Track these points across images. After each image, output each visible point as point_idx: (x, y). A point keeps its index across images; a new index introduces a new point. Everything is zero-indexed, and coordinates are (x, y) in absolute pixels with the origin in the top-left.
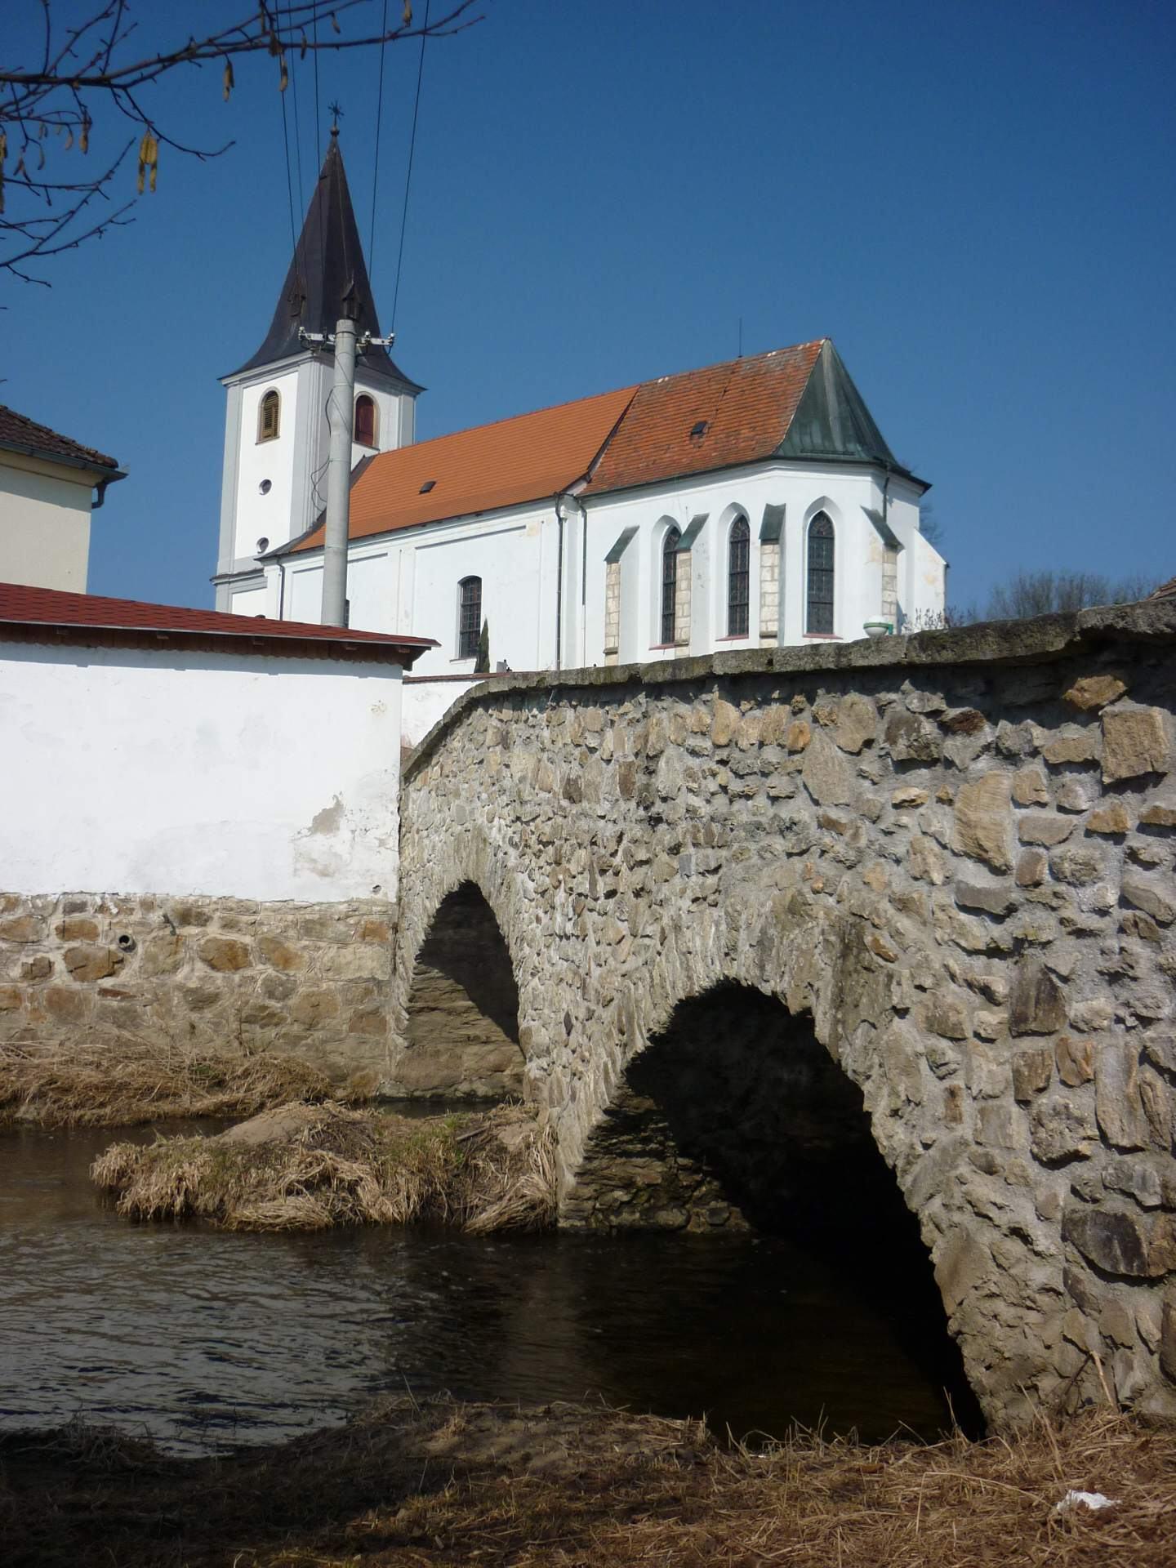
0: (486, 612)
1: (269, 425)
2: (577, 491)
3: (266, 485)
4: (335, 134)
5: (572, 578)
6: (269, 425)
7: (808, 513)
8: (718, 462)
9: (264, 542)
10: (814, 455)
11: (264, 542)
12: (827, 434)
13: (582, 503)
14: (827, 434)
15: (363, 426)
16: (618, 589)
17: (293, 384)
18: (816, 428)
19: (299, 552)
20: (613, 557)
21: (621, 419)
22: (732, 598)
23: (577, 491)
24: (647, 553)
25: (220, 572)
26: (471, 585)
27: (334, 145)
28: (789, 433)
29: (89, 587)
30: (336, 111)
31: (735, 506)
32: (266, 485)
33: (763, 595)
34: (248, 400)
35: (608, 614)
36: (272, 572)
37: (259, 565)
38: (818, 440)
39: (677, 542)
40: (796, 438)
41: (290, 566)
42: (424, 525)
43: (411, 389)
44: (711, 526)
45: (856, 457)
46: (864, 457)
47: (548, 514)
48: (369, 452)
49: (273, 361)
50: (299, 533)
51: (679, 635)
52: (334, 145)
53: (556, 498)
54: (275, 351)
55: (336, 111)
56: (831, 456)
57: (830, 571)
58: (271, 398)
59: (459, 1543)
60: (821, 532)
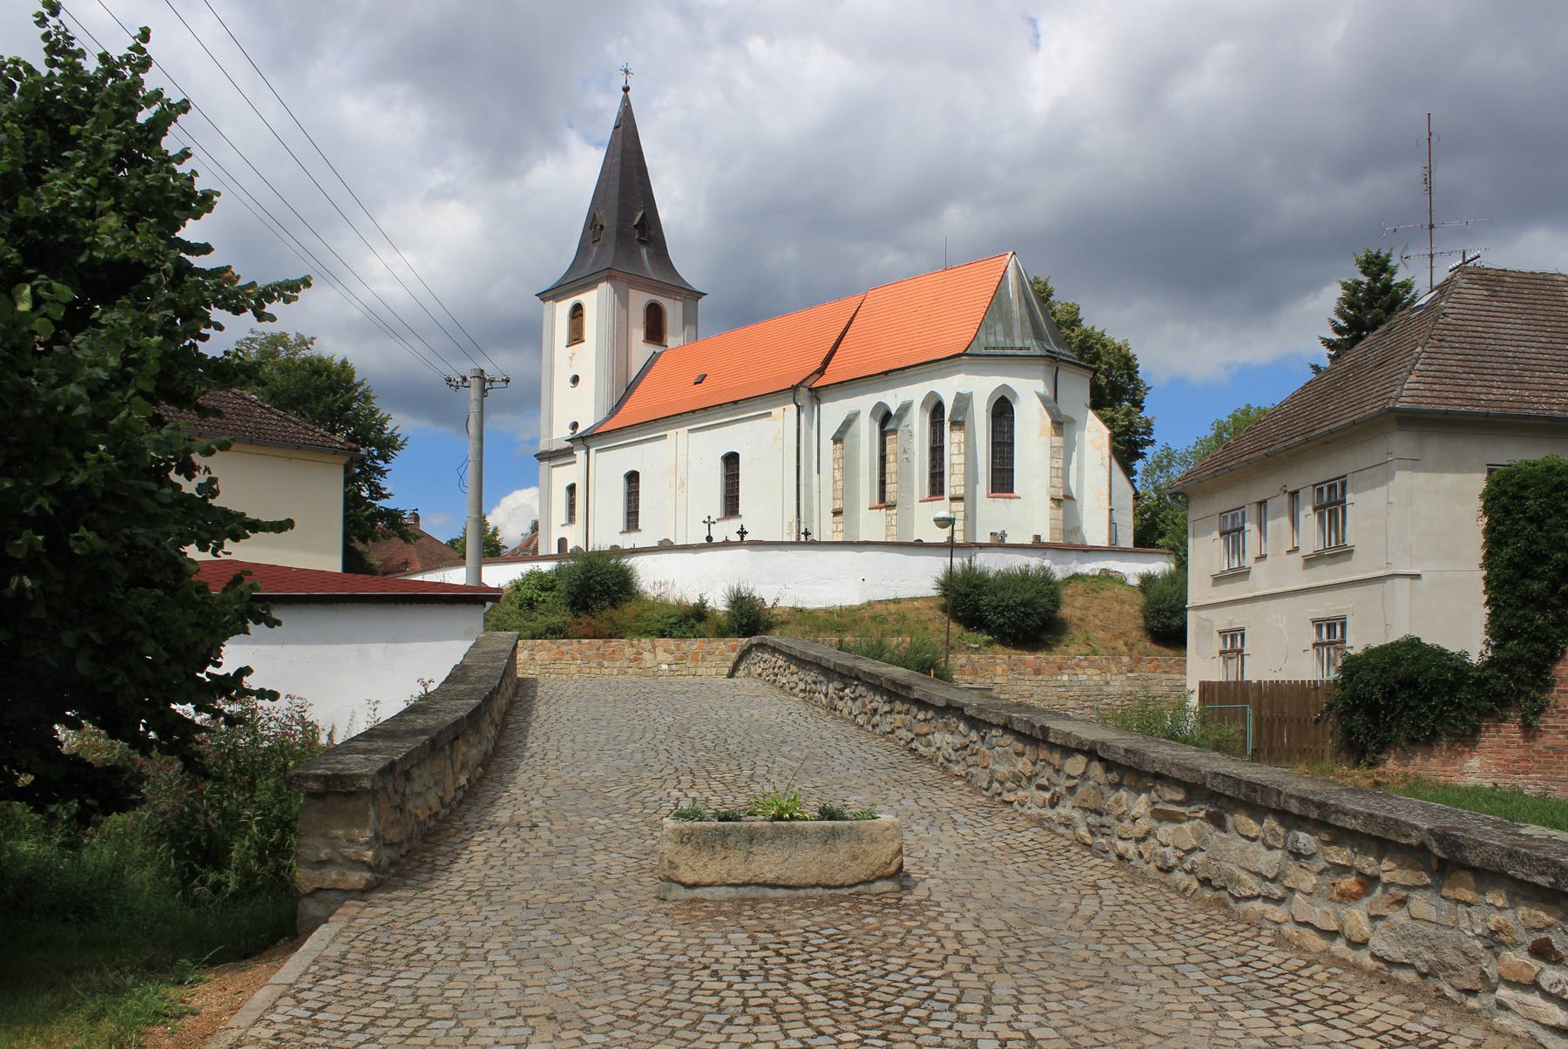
1: (576, 336)
3: (575, 380)
5: (808, 451)
6: (576, 336)
9: (575, 426)
11: (575, 426)
12: (1009, 333)
14: (1009, 333)
16: (847, 466)
20: (837, 439)
22: (637, 500)
24: (866, 430)
27: (626, 99)
29: (598, 145)
31: (933, 394)
32: (575, 380)
33: (952, 465)
35: (835, 482)
38: (1001, 338)
39: (886, 420)
40: (982, 336)
45: (1031, 352)
46: (1039, 352)
50: (601, 418)
51: (889, 498)
52: (626, 99)
56: (1009, 352)
57: (637, 493)
60: (1002, 410)
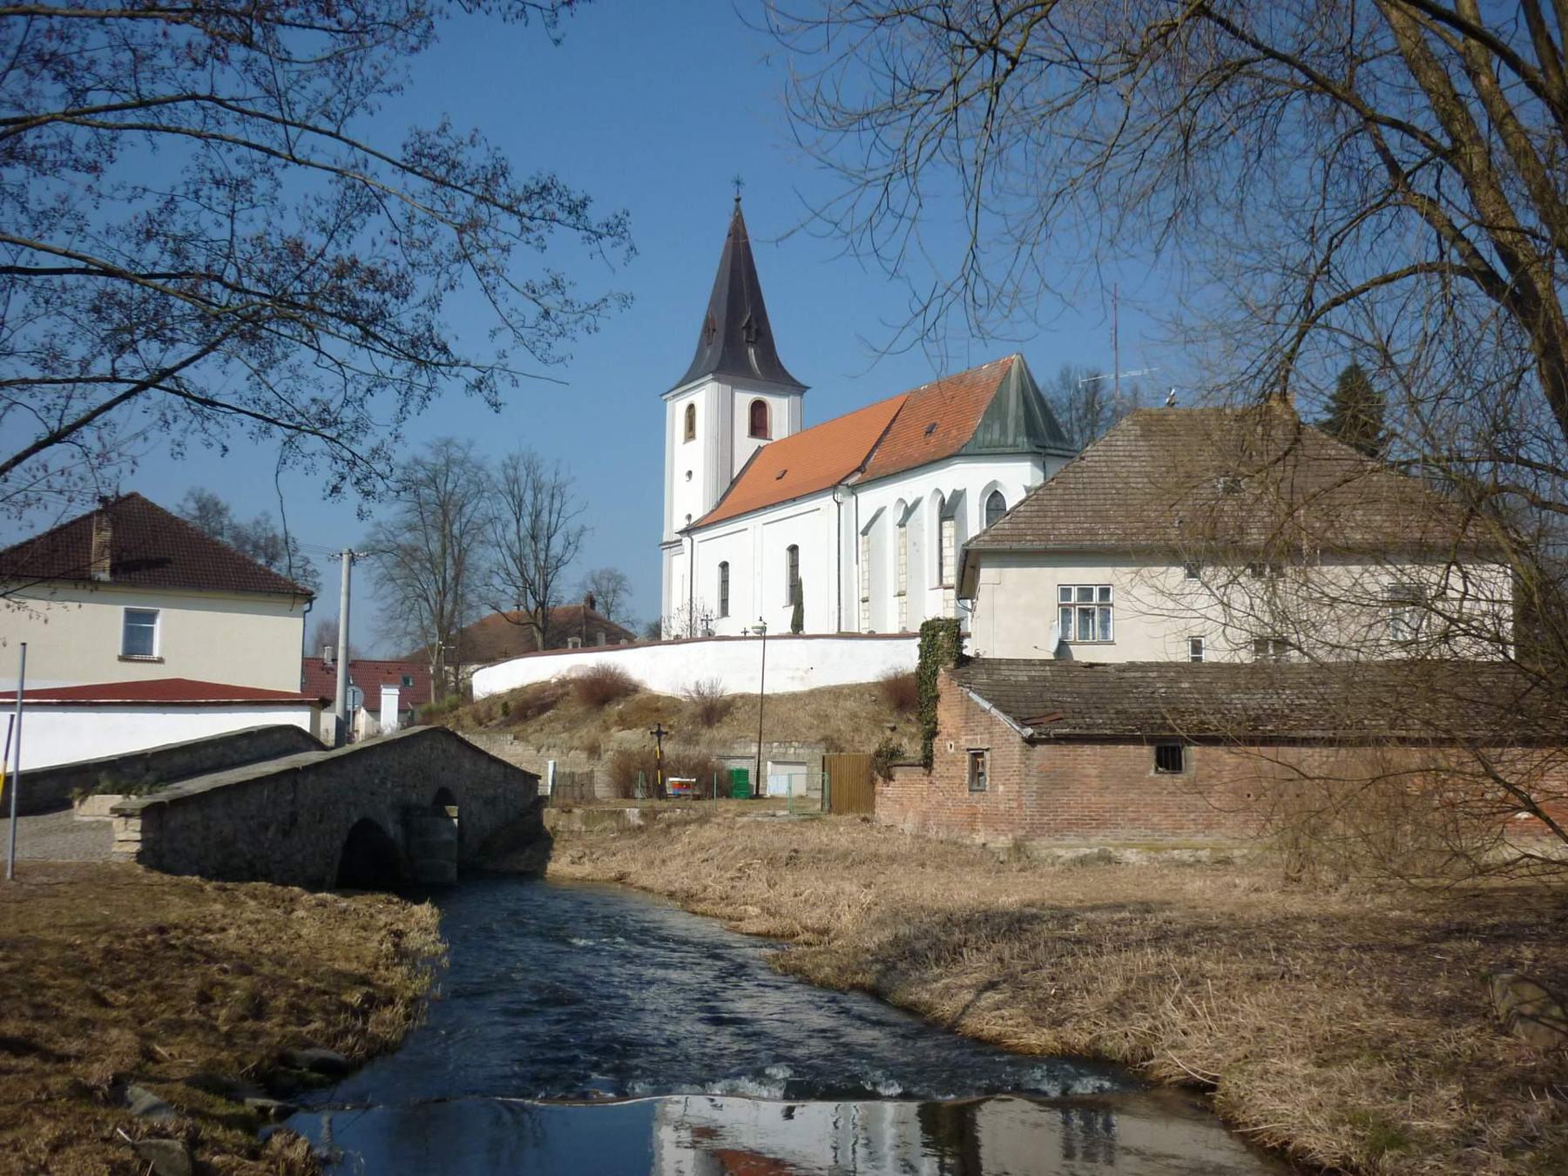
0: (801, 573)
2: (851, 481)
3: (690, 474)
4: (738, 200)
7: (983, 494)
8: (921, 461)
9: (689, 517)
10: (992, 450)
11: (689, 517)
12: (1004, 431)
13: (854, 489)
14: (1004, 431)
15: (759, 422)
17: (704, 396)
18: (997, 427)
19: (715, 523)
21: (894, 420)
23: (851, 481)
25: (665, 539)
26: (793, 549)
27: (738, 209)
28: (975, 433)
30: (738, 183)
32: (690, 474)
34: (678, 409)
36: (686, 541)
37: (678, 537)
38: (996, 436)
41: (697, 537)
42: (765, 508)
43: (797, 388)
44: (924, 505)
47: (826, 502)
48: (762, 443)
49: (259, 781)
52: (738, 209)
53: (834, 488)
54: (691, 377)
55: (738, 183)
56: (999, 450)
58: (691, 407)
59: (151, 11)
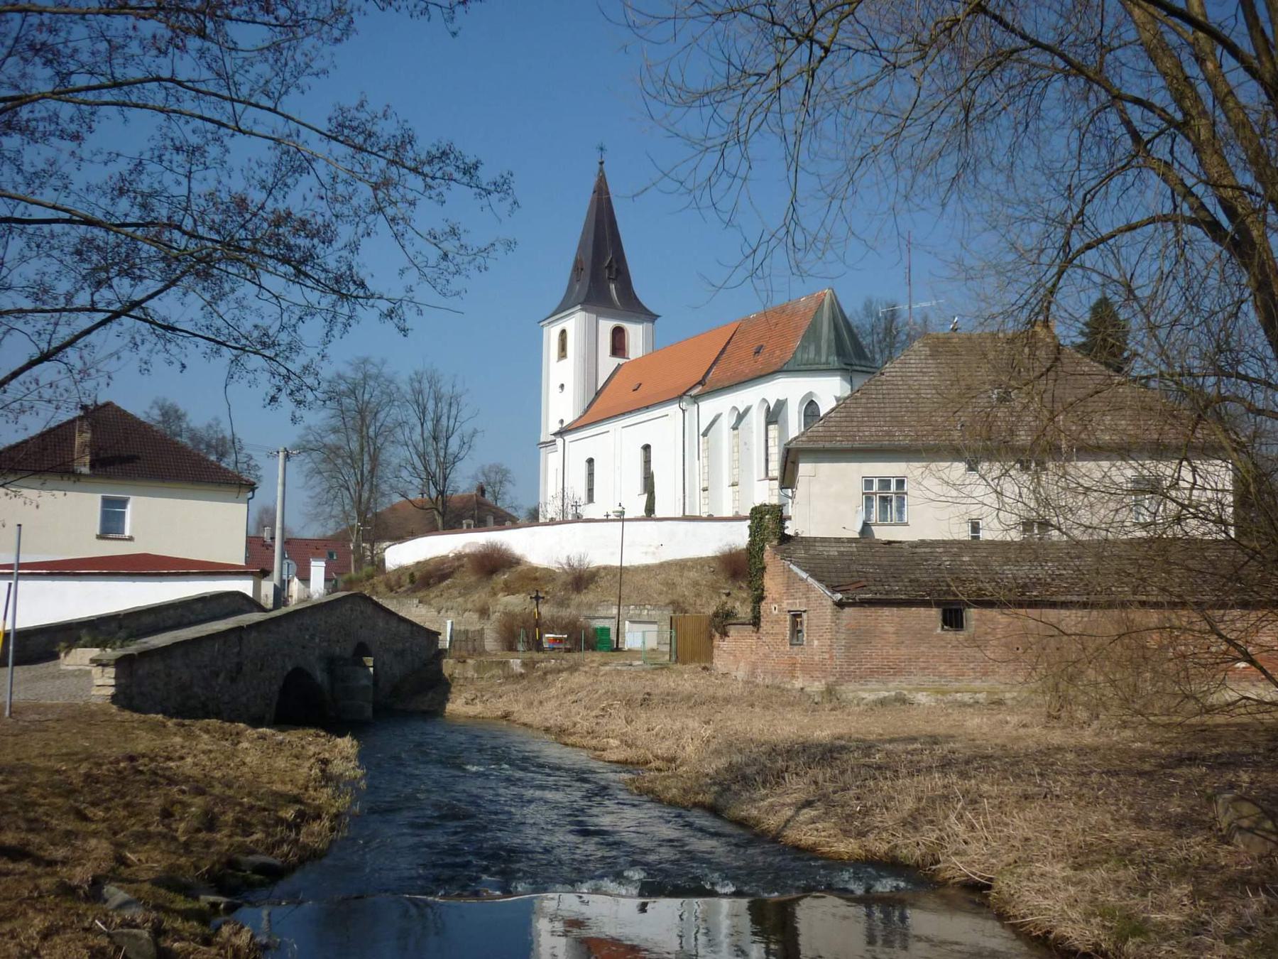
0: (653, 467)
2: (693, 392)
3: (562, 386)
4: (601, 163)
7: (801, 403)
8: (750, 376)
9: (562, 421)
10: (809, 367)
11: (562, 421)
12: (818, 352)
13: (696, 399)
14: (818, 352)
15: (618, 344)
17: (574, 323)
18: (812, 348)
19: (583, 427)
21: (728, 343)
23: (693, 392)
25: (542, 440)
26: (647, 448)
27: (601, 170)
28: (795, 353)
30: (602, 149)
32: (562, 386)
34: (552, 333)
36: (559, 441)
37: (553, 438)
38: (812, 355)
41: (568, 438)
42: (623, 414)
43: (650, 317)
44: (753, 412)
47: (673, 410)
48: (621, 361)
49: (211, 637)
52: (601, 170)
53: (680, 398)
54: (564, 308)
55: (602, 149)
56: (814, 367)
58: (563, 332)
59: (123, 9)
